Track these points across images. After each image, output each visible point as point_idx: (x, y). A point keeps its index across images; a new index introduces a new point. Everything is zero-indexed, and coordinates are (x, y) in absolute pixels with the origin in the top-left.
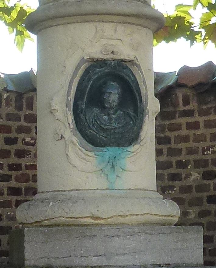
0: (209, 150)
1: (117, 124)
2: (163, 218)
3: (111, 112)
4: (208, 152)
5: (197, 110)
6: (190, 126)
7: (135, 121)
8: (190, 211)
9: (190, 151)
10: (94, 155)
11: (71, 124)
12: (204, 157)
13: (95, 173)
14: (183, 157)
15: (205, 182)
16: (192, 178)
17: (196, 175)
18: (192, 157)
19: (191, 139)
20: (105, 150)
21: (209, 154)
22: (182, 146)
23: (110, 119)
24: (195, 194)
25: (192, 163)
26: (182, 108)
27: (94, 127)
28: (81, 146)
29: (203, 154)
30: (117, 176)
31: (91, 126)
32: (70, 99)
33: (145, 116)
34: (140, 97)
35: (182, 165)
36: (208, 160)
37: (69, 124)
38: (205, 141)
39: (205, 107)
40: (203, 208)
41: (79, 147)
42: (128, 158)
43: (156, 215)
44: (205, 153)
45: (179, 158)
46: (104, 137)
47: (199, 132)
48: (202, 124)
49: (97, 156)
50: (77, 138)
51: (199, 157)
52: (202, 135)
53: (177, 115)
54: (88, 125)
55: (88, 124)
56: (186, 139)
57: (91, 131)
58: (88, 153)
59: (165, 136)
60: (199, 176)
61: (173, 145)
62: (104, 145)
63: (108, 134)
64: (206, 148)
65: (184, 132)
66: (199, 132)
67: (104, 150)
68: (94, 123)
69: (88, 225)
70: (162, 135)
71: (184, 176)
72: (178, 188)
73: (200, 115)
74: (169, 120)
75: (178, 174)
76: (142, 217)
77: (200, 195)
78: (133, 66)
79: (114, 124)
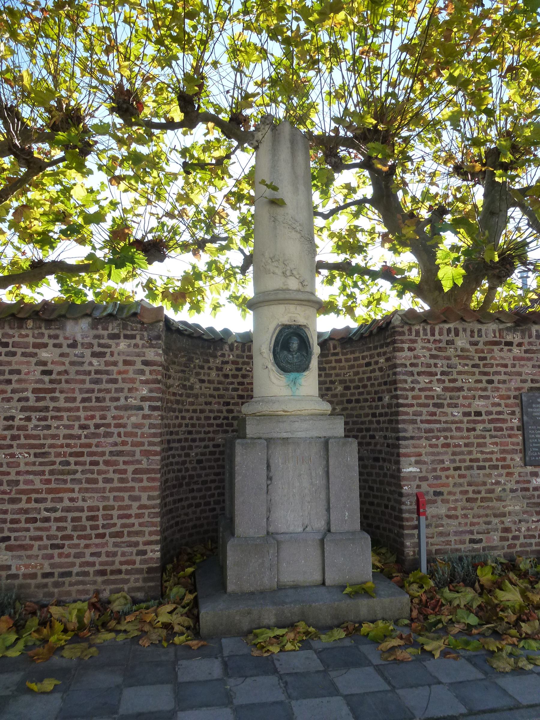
14: (333, 378)
22: (332, 372)
24: (339, 398)
35: (332, 382)
56: (334, 368)
61: (327, 372)
65: (334, 364)
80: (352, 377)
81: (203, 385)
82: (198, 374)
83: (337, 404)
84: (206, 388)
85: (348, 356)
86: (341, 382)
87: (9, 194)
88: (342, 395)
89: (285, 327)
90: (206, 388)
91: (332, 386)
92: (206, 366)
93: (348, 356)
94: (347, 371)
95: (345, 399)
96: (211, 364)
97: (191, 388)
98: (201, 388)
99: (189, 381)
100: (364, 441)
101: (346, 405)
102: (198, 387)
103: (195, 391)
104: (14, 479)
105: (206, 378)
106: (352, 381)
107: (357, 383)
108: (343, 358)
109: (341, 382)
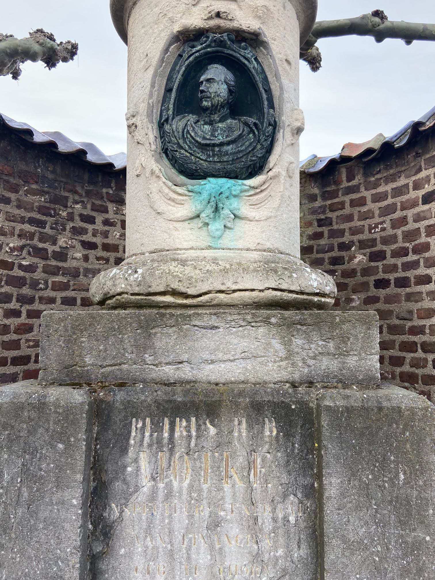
0: (378, 228)
1: (224, 137)
2: (295, 296)
3: (216, 117)
4: (377, 230)
5: (363, 185)
6: (354, 203)
7: (257, 133)
8: (354, 297)
9: (354, 231)
10: (187, 193)
11: (152, 143)
12: (371, 236)
13: (189, 222)
14: (347, 238)
15: (373, 264)
16: (356, 260)
17: (361, 257)
18: (355, 238)
19: (356, 218)
20: (205, 182)
21: (378, 232)
22: (346, 226)
23: (214, 130)
24: (359, 278)
25: (357, 244)
26: (345, 184)
27: (186, 143)
28: (167, 178)
29: (370, 232)
30: (225, 226)
31: (181, 142)
32: (153, 102)
33: (279, 131)
34: (268, 91)
35: (344, 247)
36: (376, 239)
37: (150, 143)
38: (373, 217)
39: (373, 179)
40: (370, 294)
41: (164, 180)
42: (244, 197)
43: (291, 292)
44: (373, 231)
45: (341, 240)
46: (202, 160)
47: (364, 209)
48: (369, 199)
49: (191, 194)
50: (161, 166)
51: (365, 236)
52: (369, 211)
53: (340, 193)
54: (176, 141)
55: (176, 139)
56: (349, 218)
57: (183, 151)
58: (179, 189)
59: (326, 218)
60: (365, 257)
61: (335, 227)
62: (204, 176)
63: (210, 155)
64: (373, 225)
65: (347, 210)
66: (364, 209)
67: (202, 183)
68: (185, 136)
69: (168, 306)
70: (323, 217)
71: (346, 259)
72: (340, 272)
73: (366, 189)
74: (331, 199)
75: (340, 257)
76: (262, 294)
77: (365, 279)
78: (259, 48)
79: (220, 137)
80: (390, 232)
81: (92, 254)
82: (76, 231)
83: (354, 291)
84: (98, 259)
85: (381, 189)
86: (363, 245)
87: (420, 326)
88: (366, 271)
89: (188, 37)
90: (98, 259)
91: (344, 253)
92: (99, 218)
93: (381, 189)
94: (377, 220)
95: (372, 279)
96: (111, 215)
97: (62, 256)
98: (86, 258)
99: (54, 243)
100: (420, 372)
101: (373, 291)
102: (79, 255)
103: (71, 264)
104: (379, 263)
105: (98, 240)
106: (387, 240)
107: (400, 244)
108: (368, 194)
109: (363, 245)
